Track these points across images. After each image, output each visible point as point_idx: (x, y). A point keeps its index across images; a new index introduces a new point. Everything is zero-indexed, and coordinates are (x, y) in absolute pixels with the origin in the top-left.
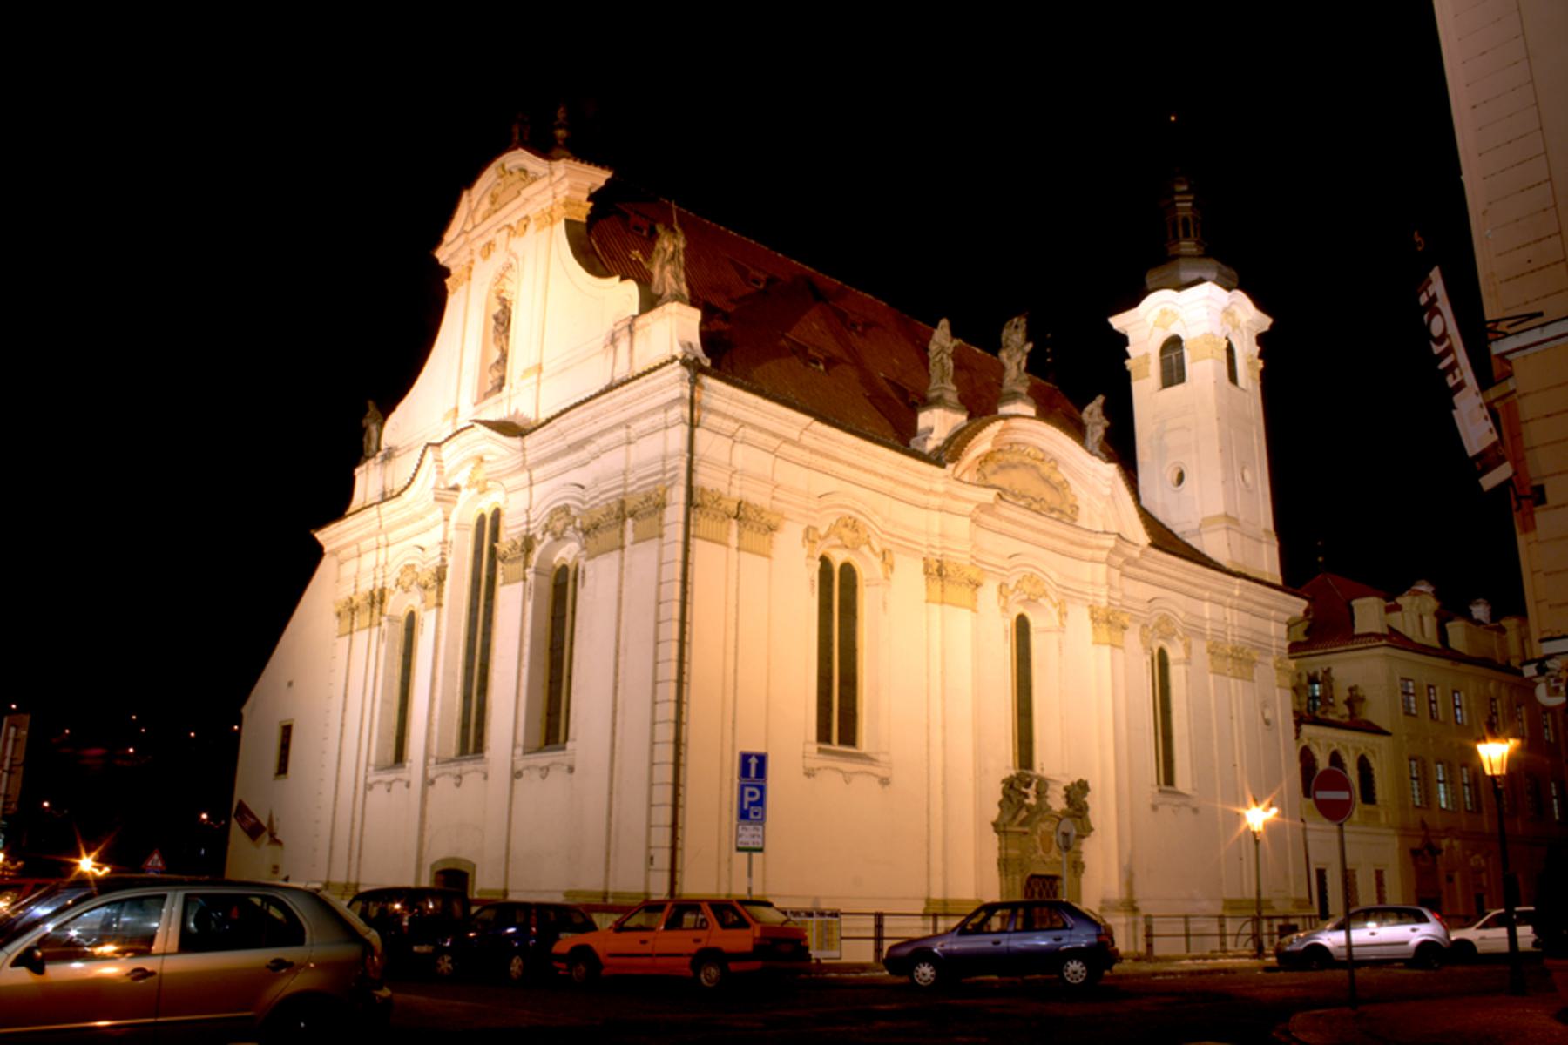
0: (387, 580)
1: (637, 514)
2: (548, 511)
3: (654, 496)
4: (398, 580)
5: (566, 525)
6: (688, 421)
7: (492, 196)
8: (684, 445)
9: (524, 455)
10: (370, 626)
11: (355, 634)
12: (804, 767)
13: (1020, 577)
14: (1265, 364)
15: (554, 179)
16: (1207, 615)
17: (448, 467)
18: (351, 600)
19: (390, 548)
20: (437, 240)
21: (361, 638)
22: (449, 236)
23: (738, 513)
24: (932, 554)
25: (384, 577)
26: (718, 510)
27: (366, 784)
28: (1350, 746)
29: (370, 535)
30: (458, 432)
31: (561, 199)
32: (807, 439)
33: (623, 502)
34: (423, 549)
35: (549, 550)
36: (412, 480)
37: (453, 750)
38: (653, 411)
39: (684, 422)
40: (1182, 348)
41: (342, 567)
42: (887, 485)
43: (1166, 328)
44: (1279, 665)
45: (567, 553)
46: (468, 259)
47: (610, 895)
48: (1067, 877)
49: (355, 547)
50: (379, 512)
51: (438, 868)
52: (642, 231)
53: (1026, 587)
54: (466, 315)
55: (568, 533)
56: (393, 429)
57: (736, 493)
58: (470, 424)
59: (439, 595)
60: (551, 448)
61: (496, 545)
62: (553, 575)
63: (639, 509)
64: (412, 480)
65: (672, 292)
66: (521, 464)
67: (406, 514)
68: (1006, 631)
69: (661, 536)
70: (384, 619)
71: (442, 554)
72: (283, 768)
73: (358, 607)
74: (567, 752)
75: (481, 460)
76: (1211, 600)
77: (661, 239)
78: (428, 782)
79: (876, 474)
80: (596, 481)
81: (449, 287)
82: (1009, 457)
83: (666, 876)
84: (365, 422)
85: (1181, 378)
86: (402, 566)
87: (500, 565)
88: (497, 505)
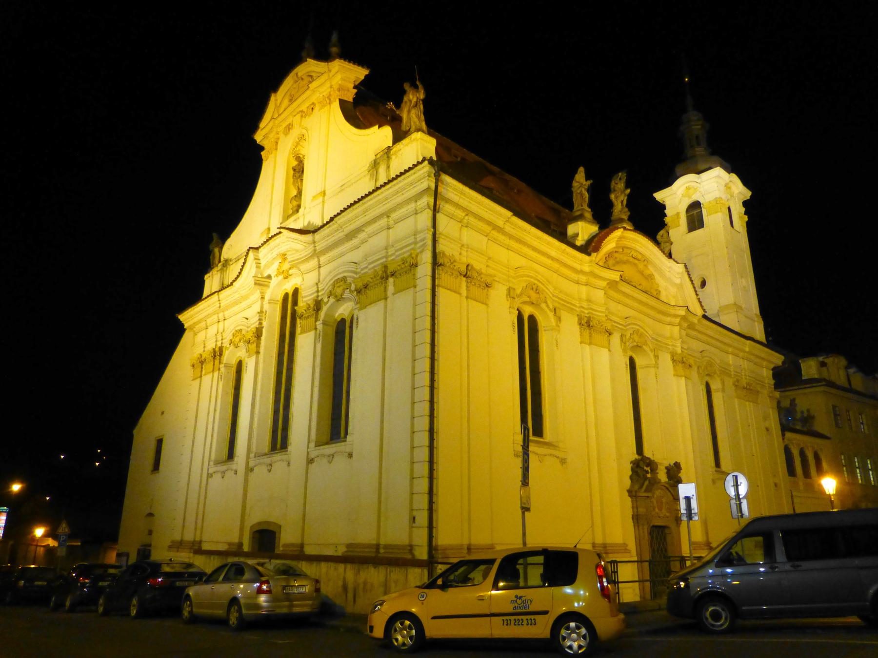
0: (224, 341)
1: (397, 274)
2: (332, 282)
3: (408, 260)
4: (231, 340)
6: (432, 208)
7: (291, 95)
8: (429, 223)
9: (315, 246)
10: (213, 371)
11: (203, 377)
13: (631, 331)
14: (748, 218)
17: (263, 263)
18: (201, 355)
19: (226, 321)
20: (255, 127)
21: (207, 379)
23: (467, 273)
25: (222, 339)
27: (208, 474)
29: (214, 313)
30: (270, 238)
31: (336, 87)
32: (508, 228)
33: (386, 267)
34: (247, 319)
35: (333, 308)
36: (240, 273)
38: (408, 201)
39: (429, 207)
40: (701, 208)
41: (196, 336)
42: (555, 265)
43: (690, 197)
44: (771, 395)
45: (344, 310)
47: (381, 546)
48: (673, 526)
49: (204, 322)
53: (636, 338)
54: (274, 170)
56: (229, 249)
57: (464, 260)
58: (278, 231)
59: (258, 346)
60: (333, 239)
61: (296, 308)
62: (335, 325)
63: (398, 270)
64: (240, 273)
65: (416, 127)
66: (313, 252)
67: (237, 296)
68: (627, 365)
69: (415, 287)
73: (205, 360)
74: (347, 443)
76: (733, 354)
77: (407, 95)
78: (249, 470)
79: (549, 257)
80: (365, 257)
81: (263, 157)
82: (621, 256)
83: (425, 532)
86: (234, 331)
87: (298, 321)
88: (297, 287)
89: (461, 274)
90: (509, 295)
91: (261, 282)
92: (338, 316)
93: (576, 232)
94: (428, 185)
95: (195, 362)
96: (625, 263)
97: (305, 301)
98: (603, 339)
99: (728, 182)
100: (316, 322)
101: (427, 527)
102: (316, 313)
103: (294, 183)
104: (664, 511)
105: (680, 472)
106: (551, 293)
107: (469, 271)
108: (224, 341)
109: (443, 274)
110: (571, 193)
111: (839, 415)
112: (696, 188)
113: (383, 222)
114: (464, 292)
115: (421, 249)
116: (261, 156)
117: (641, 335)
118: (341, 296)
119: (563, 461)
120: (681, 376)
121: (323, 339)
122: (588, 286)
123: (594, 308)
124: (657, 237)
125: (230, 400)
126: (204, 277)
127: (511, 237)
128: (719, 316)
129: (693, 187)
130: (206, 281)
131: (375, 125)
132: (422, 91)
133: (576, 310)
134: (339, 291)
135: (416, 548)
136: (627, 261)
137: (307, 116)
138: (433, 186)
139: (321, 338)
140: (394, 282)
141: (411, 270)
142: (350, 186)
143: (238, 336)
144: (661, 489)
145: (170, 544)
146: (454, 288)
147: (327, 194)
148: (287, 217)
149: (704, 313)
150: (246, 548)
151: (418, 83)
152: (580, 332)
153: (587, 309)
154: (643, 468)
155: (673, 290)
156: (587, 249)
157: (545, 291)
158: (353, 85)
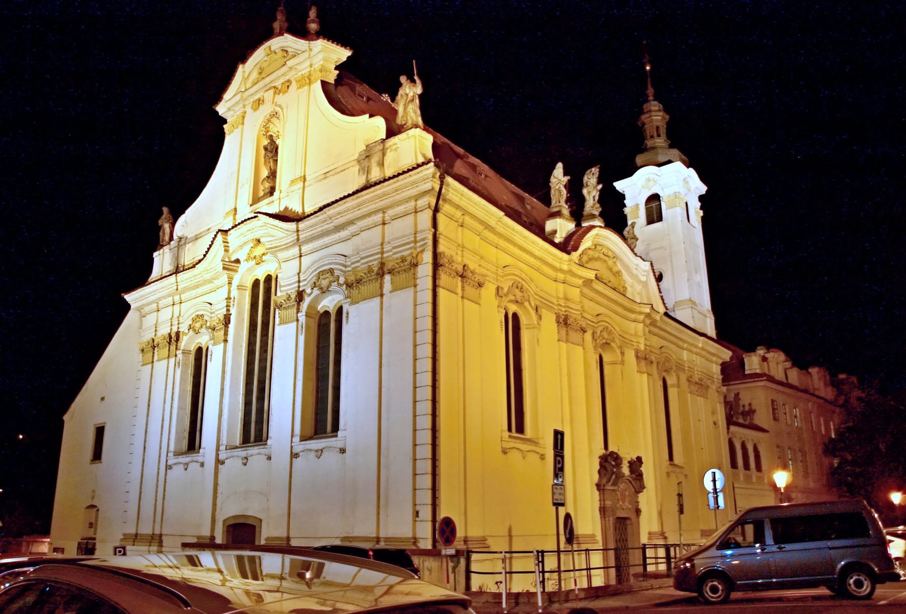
0: (180, 326)
4: (190, 325)
5: (331, 282)
12: (502, 447)
18: (153, 340)
19: (182, 304)
20: (218, 99)
21: (160, 366)
22: (227, 96)
26: (452, 269)
34: (211, 304)
35: (316, 300)
37: (238, 439)
40: (660, 201)
44: (719, 390)
45: (328, 303)
46: (242, 110)
47: (382, 539)
51: (229, 523)
52: (363, 98)
53: (605, 335)
55: (334, 287)
58: (253, 215)
59: (226, 334)
63: (396, 268)
69: (415, 286)
71: (227, 306)
72: (97, 455)
75: (259, 241)
78: (219, 462)
84: (160, 222)
85: (660, 219)
86: (194, 316)
88: (270, 273)
89: (457, 274)
90: (498, 294)
91: (231, 265)
92: (321, 308)
93: (554, 228)
95: (145, 346)
103: (265, 163)
104: (627, 504)
105: (641, 467)
106: (533, 290)
108: (180, 326)
111: (777, 409)
113: (378, 218)
114: (459, 291)
115: (422, 248)
117: (610, 333)
120: (643, 373)
122: (565, 284)
126: (153, 255)
127: (501, 236)
129: (654, 180)
133: (554, 308)
138: (437, 188)
140: (391, 280)
141: (410, 269)
142: (336, 174)
144: (625, 482)
147: (307, 179)
150: (219, 540)
151: (416, 78)
152: (558, 329)
155: (638, 287)
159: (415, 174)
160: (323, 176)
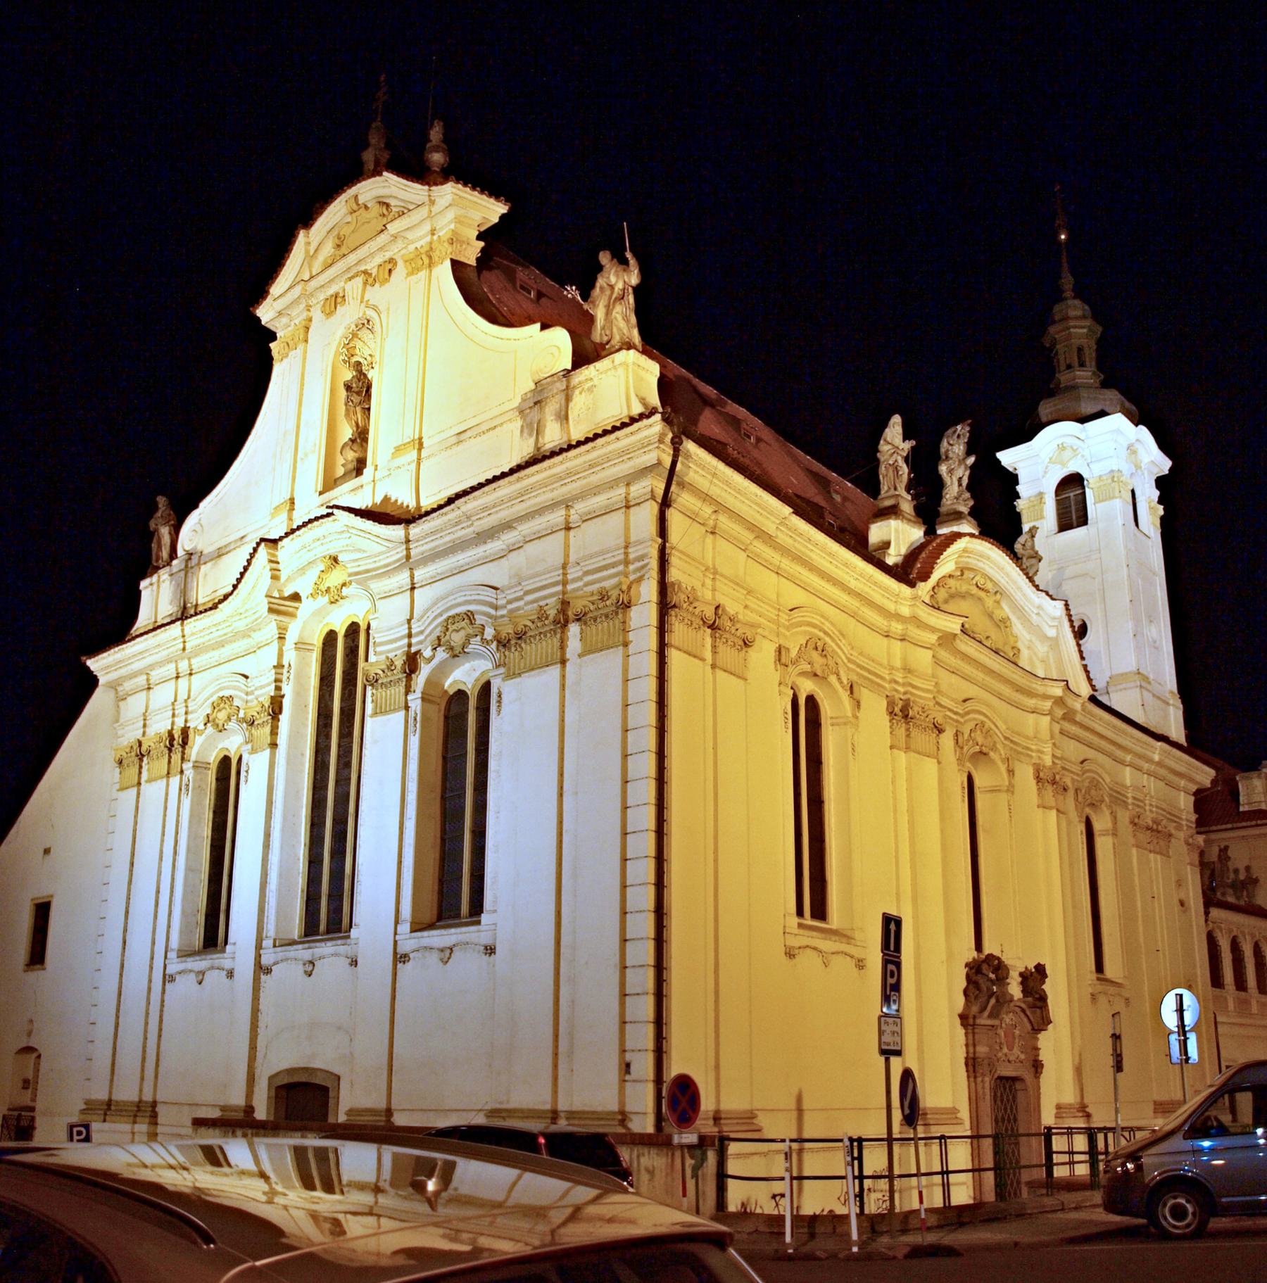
0: (189, 717)
4: (208, 716)
8: (652, 527)
13: (971, 725)
15: (435, 209)
16: (1128, 783)
20: (261, 293)
21: (153, 792)
22: (276, 289)
23: (715, 622)
24: (896, 690)
28: (1246, 931)
34: (247, 677)
35: (442, 670)
37: (296, 927)
39: (653, 498)
40: (1083, 487)
42: (853, 603)
45: (464, 676)
46: (305, 315)
47: (562, 1115)
48: (1028, 1076)
50: (183, 630)
53: (979, 737)
59: (274, 732)
65: (621, 338)
69: (626, 644)
70: (188, 766)
71: (276, 680)
72: (37, 956)
75: (335, 560)
77: (604, 273)
78: (261, 969)
81: (275, 353)
84: (152, 525)
85: (1083, 520)
86: (215, 698)
90: (779, 660)
92: (451, 685)
93: (885, 538)
94: (658, 460)
95: (124, 754)
96: (963, 596)
97: (381, 653)
98: (929, 741)
99: (1134, 441)
100: (407, 693)
101: (654, 1081)
102: (406, 677)
104: (1016, 1051)
107: (719, 618)
108: (189, 717)
109: (677, 624)
110: (876, 463)
112: (1077, 449)
113: (557, 517)
116: (270, 350)
117: (988, 733)
118: (463, 649)
119: (861, 964)
120: (1050, 808)
121: (423, 727)
123: (914, 683)
124: (1015, 546)
125: (207, 831)
128: (1108, 693)
130: (143, 594)
131: (534, 322)
132: (636, 272)
134: (457, 639)
135: (633, 1117)
136: (966, 592)
137: (377, 285)
138: (667, 461)
139: (418, 725)
141: (617, 613)
142: (479, 435)
143: (224, 708)
144: (1014, 1012)
145: (84, 1107)
146: (729, 666)
148: (330, 483)
149: (1092, 692)
151: (629, 255)
152: (891, 727)
153: (904, 685)
154: (987, 976)
156: (908, 575)
157: (837, 653)
158: (477, 233)
159: (627, 436)
160: (454, 440)
